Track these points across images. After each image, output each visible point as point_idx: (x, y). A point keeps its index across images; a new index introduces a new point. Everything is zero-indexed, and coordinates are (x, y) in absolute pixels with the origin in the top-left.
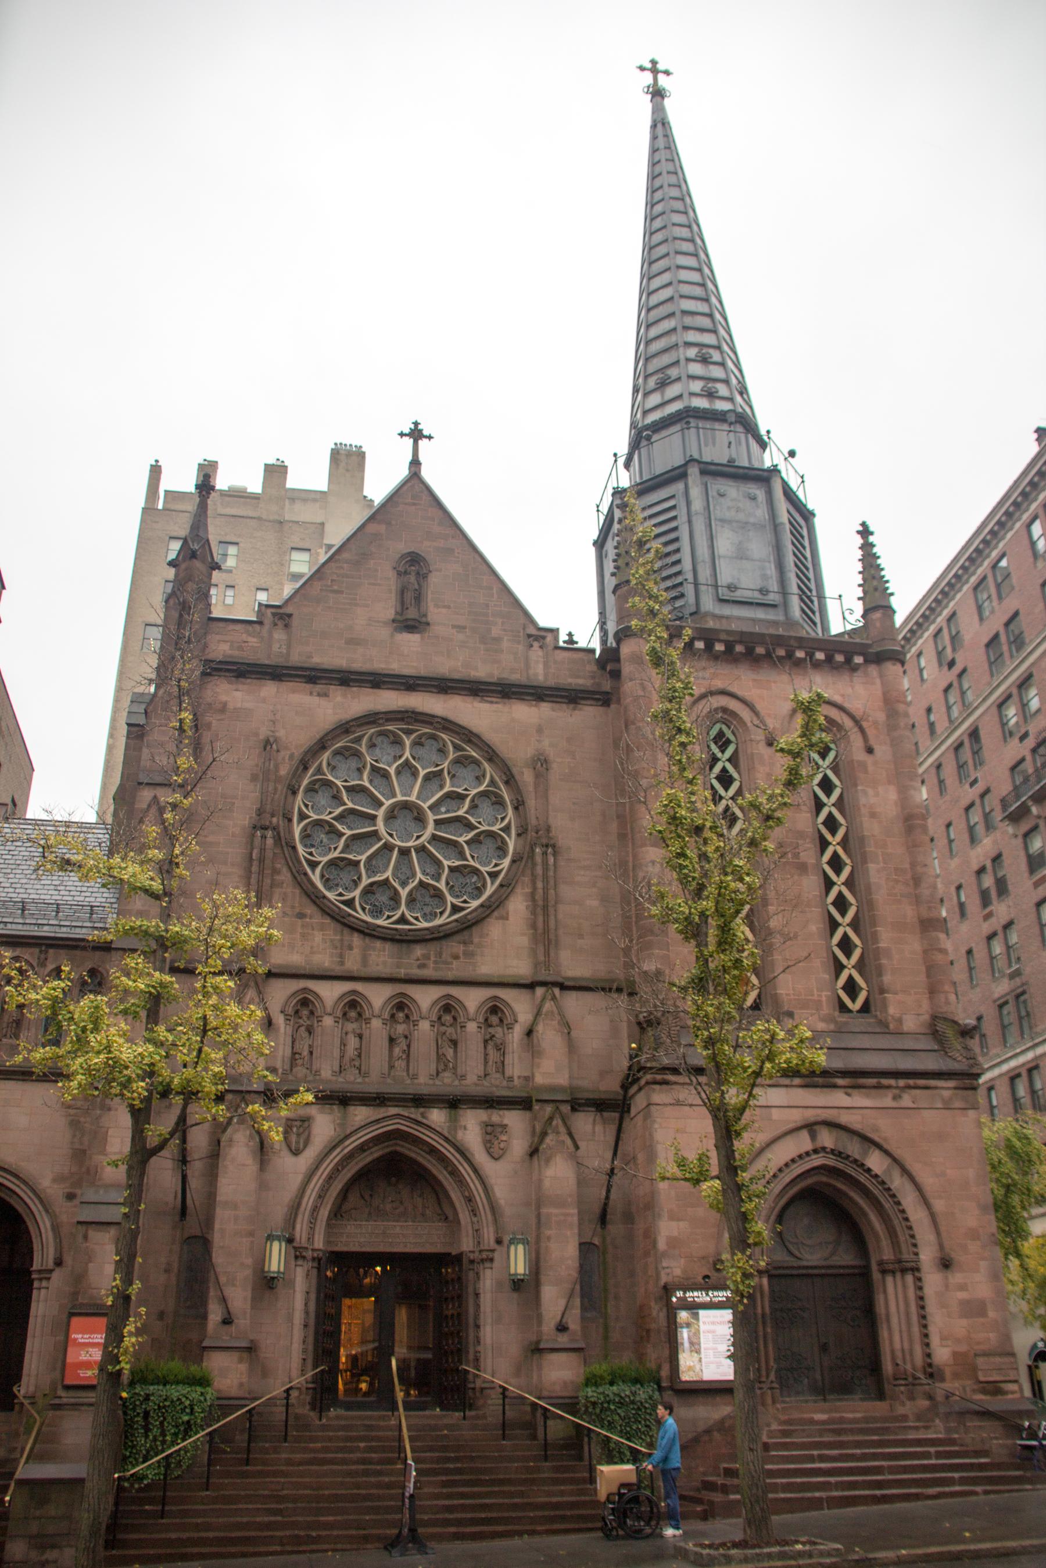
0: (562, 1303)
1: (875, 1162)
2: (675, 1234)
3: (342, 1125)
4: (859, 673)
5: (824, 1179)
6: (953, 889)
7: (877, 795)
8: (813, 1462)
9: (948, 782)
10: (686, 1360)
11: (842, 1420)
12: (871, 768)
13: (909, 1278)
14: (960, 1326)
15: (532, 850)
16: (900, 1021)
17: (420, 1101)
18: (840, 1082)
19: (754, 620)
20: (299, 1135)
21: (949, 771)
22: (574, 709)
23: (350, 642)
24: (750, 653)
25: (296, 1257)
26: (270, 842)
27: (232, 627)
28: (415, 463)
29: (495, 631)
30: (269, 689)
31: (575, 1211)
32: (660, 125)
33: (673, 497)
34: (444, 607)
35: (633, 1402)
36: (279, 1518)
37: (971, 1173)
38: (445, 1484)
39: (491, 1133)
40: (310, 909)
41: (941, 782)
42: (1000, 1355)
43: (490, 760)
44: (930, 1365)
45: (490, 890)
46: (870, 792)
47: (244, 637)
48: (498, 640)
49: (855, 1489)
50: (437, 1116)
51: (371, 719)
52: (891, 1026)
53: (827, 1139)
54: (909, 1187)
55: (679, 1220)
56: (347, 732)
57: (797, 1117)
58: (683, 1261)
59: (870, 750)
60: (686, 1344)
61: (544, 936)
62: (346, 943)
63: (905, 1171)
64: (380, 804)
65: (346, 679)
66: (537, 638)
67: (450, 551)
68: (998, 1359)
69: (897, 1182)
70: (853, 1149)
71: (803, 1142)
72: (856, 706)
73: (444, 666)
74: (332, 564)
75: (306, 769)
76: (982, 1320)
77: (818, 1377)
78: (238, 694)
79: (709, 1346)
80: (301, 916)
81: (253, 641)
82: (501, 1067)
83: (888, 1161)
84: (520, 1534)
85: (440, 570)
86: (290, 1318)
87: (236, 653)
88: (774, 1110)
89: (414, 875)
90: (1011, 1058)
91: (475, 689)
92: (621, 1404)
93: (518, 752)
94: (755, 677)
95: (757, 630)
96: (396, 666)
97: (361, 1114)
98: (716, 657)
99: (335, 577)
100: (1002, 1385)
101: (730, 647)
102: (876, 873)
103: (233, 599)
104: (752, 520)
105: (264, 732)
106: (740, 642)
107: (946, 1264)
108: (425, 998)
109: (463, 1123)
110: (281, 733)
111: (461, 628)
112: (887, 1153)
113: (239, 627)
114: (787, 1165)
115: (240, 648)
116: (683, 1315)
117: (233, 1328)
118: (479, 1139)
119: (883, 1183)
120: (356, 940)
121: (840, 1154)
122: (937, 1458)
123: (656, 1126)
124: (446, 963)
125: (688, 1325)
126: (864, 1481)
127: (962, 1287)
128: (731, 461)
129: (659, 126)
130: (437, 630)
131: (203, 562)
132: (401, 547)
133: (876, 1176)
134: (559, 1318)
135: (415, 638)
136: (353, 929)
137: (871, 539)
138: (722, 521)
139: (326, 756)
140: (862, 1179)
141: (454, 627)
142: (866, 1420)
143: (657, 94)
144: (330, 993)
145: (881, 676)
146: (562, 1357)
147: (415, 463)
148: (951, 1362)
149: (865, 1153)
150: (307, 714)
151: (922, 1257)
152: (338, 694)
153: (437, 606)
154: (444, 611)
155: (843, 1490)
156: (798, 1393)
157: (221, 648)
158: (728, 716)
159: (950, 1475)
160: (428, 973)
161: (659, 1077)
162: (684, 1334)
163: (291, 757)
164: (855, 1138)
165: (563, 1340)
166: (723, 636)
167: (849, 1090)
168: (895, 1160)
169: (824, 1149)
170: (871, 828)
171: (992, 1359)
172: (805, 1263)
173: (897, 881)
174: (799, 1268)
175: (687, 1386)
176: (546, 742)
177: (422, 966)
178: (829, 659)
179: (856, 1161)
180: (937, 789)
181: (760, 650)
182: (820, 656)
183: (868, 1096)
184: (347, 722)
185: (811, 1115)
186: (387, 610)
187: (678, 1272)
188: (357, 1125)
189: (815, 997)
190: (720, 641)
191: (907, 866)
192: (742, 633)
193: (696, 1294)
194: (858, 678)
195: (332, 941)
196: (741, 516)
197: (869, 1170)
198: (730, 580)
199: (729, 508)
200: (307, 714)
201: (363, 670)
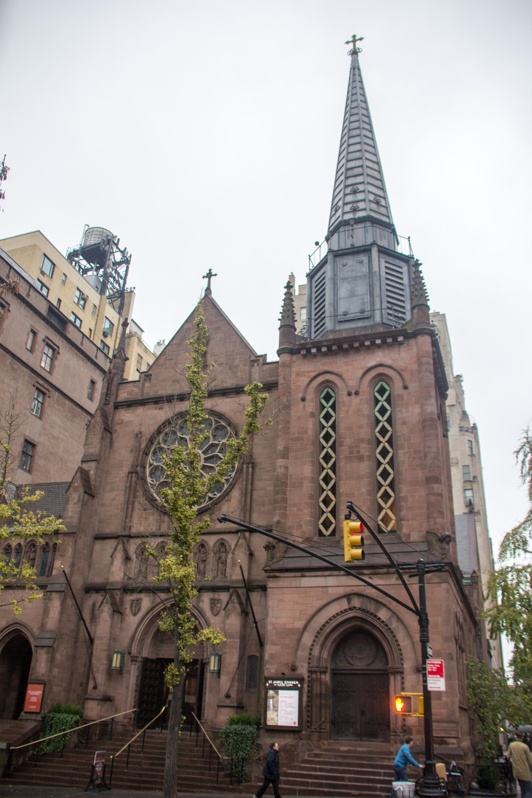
0: (229, 684)
2: (274, 652)
3: (153, 602)
4: (404, 345)
5: (359, 623)
7: (408, 411)
8: (316, 771)
10: (270, 714)
11: (355, 752)
12: (405, 397)
13: (399, 677)
15: (242, 466)
16: (409, 536)
18: (366, 572)
19: (354, 329)
20: (136, 607)
24: (340, 348)
25: (132, 661)
26: (134, 478)
28: (208, 290)
29: (236, 362)
30: (140, 410)
31: (238, 640)
32: (355, 69)
35: (242, 734)
36: (77, 772)
38: (152, 764)
39: (214, 602)
42: (447, 722)
43: (229, 425)
44: (404, 725)
45: (226, 486)
46: (404, 410)
49: (322, 787)
53: (356, 602)
54: (401, 627)
55: (276, 645)
57: (341, 591)
58: (276, 665)
59: (406, 388)
60: (271, 707)
61: (247, 506)
65: (169, 399)
66: (255, 361)
68: (445, 725)
69: (394, 625)
70: (371, 607)
71: (344, 604)
72: (400, 364)
74: (169, 347)
75: (152, 443)
77: (358, 728)
78: (128, 415)
79: (285, 708)
81: (136, 390)
82: (224, 573)
83: (389, 614)
84: (155, 789)
85: (214, 339)
86: (128, 687)
87: (129, 396)
88: (329, 589)
92: (236, 734)
94: (345, 360)
95: (357, 333)
98: (325, 354)
100: (446, 739)
101: (329, 348)
102: (402, 456)
104: (359, 274)
105: (137, 430)
106: (334, 344)
109: (202, 599)
110: (143, 429)
112: (389, 609)
114: (334, 617)
115: (131, 394)
116: (271, 692)
117: (97, 691)
118: (209, 607)
119: (387, 625)
121: (364, 610)
122: (384, 776)
123: (269, 598)
125: (273, 697)
126: (326, 783)
128: (353, 245)
129: (356, 70)
131: (120, 359)
133: (383, 622)
134: (227, 691)
138: (343, 279)
139: (161, 437)
140: (375, 623)
142: (369, 752)
143: (355, 53)
145: (417, 344)
147: (208, 290)
148: (417, 724)
149: (377, 610)
150: (152, 417)
151: (405, 666)
155: (314, 787)
156: (347, 736)
157: (123, 395)
158: (327, 383)
159: (375, 785)
161: (272, 574)
162: (271, 702)
163: (146, 439)
164: (373, 601)
165: (228, 702)
166: (325, 343)
167: (371, 576)
168: (394, 613)
169: (355, 608)
170: (401, 430)
171: (441, 724)
172: (356, 668)
173: (414, 458)
174: (351, 670)
175: (269, 728)
178: (384, 342)
179: (372, 614)
181: (345, 346)
182: (378, 342)
183: (381, 578)
185: (348, 590)
187: (273, 671)
190: (324, 346)
191: (422, 449)
192: (334, 339)
193: (278, 682)
194: (403, 349)
196: (354, 274)
197: (379, 619)
198: (344, 310)
200: (152, 417)
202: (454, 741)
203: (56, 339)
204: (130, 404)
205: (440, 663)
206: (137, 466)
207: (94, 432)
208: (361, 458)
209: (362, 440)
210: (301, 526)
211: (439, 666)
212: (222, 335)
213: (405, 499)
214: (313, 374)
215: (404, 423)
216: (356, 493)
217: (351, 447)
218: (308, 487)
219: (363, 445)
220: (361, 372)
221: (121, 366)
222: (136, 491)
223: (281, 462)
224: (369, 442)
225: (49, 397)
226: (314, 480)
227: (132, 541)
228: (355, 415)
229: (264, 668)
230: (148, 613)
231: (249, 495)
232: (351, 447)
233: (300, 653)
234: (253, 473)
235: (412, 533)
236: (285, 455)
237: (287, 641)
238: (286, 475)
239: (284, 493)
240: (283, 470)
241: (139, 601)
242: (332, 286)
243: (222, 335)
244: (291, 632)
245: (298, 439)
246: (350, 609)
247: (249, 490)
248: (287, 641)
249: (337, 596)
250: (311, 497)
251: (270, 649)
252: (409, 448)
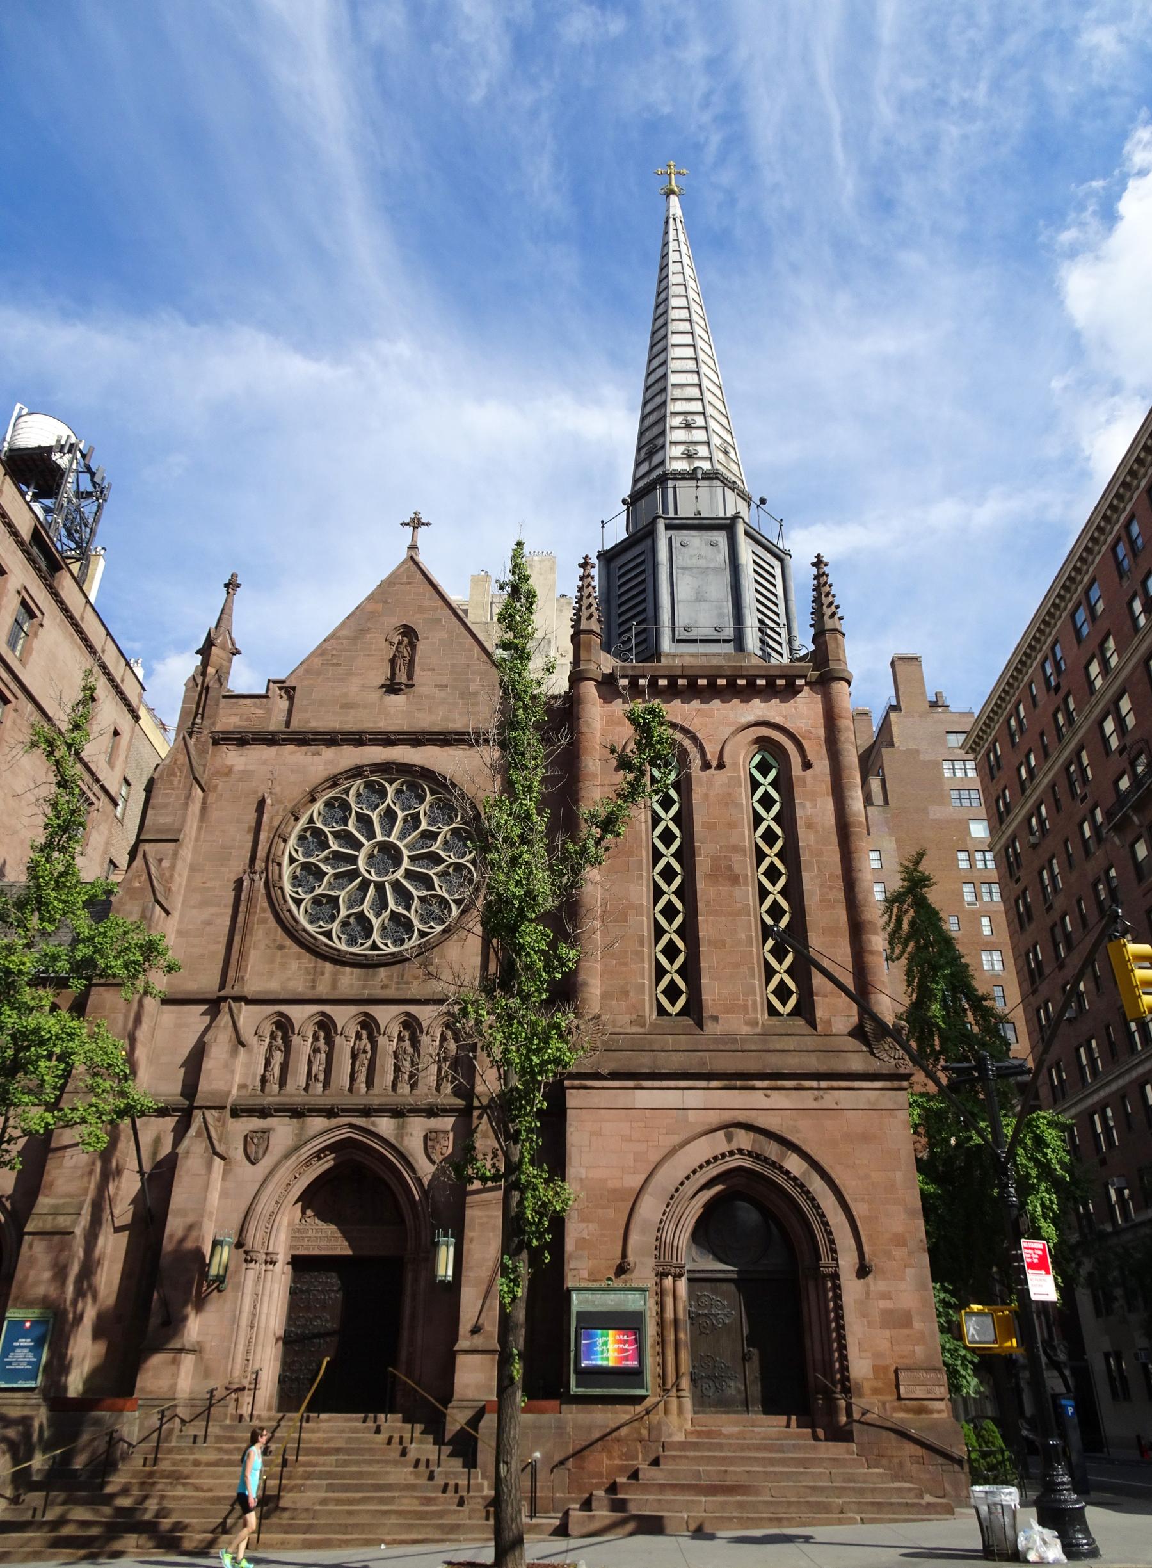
1: (794, 1164)
3: (299, 1135)
6: (1074, 902)
7: (815, 807)
9: (1063, 801)
14: (882, 1339)
16: (829, 1023)
17: (367, 1112)
18: (758, 1084)
21: (1062, 790)
23: (346, 706)
27: (242, 701)
28: (413, 547)
33: (643, 552)
34: (429, 670)
37: (899, 1176)
40: (289, 942)
41: (1057, 801)
46: (808, 804)
47: (253, 710)
48: (475, 694)
50: (385, 1126)
51: (356, 772)
52: (819, 1028)
56: (335, 785)
57: (715, 1118)
62: (318, 970)
69: (817, 1185)
70: (772, 1150)
71: (718, 1143)
73: (425, 721)
76: (906, 1331)
81: (260, 712)
85: (427, 638)
87: (245, 724)
89: (362, 903)
90: (1138, 1064)
91: (445, 739)
96: (383, 725)
97: (318, 1123)
99: (334, 652)
103: (244, 678)
104: (712, 565)
108: (385, 1015)
109: (409, 1130)
111: (442, 687)
113: (248, 701)
120: (328, 966)
124: (407, 983)
127: (886, 1296)
132: (397, 621)
133: (795, 1179)
135: (400, 699)
136: (325, 958)
137: (826, 569)
138: (684, 568)
141: (436, 686)
144: (299, 1014)
146: (477, 1358)
147: (413, 547)
149: (783, 1156)
152: (328, 753)
154: (429, 673)
157: (228, 719)
160: (390, 993)
167: (769, 1092)
169: (740, 1151)
173: (831, 888)
177: (384, 987)
179: (774, 1164)
180: (1054, 808)
184: (335, 776)
185: (728, 1116)
186: (381, 675)
188: (312, 1133)
189: (741, 1002)
195: (306, 968)
196: (703, 563)
197: (787, 1173)
199: (691, 557)
201: (354, 730)
203: (41, 596)
204: (241, 739)
205: (1041, 1246)
207: (171, 782)
210: (627, 994)
211: (1040, 1253)
212: (444, 635)
215: (810, 826)
216: (728, 940)
217: (715, 859)
221: (225, 663)
225: (16, 710)
229: (566, 1268)
230: (287, 1156)
232: (715, 859)
235: (833, 1019)
237: (611, 1213)
243: (444, 635)
244: (616, 1194)
248: (611, 1213)
249: (707, 1127)
251: (574, 1232)
252: (819, 869)
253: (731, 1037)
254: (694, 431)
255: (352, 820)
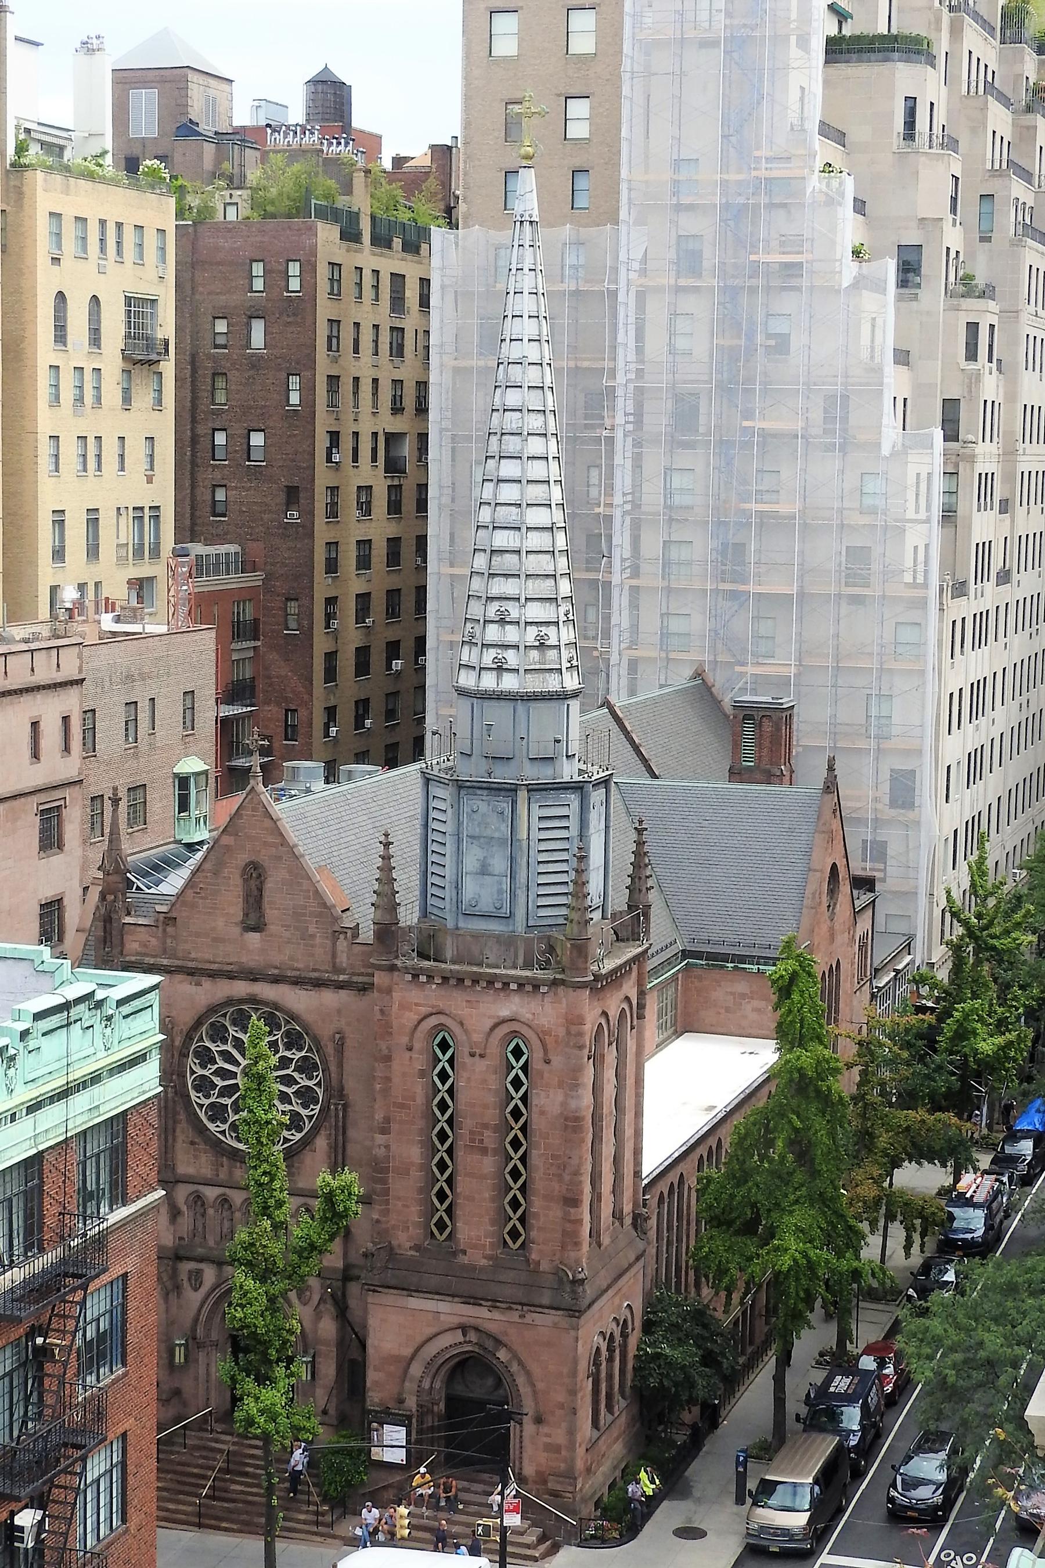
7: (548, 1097)
12: (546, 1075)
14: (543, 1457)
16: (538, 1263)
22: (364, 995)
23: (215, 940)
29: (312, 930)
46: (543, 1094)
51: (230, 1002)
57: (456, 1320)
59: (548, 1062)
63: (521, 1363)
64: (238, 1064)
67: (280, 858)
69: (515, 1368)
70: (489, 1344)
76: (556, 1455)
80: (192, 1143)
86: (196, 1379)
93: (325, 1031)
102: (536, 1158)
107: (539, 1420)
115: (145, 946)
130: (272, 928)
141: (282, 926)
144: (211, 1193)
149: (497, 1350)
152: (207, 983)
153: (271, 908)
170: (538, 1123)
173: (552, 1165)
176: (343, 1023)
183: (503, 1313)
185: (464, 1320)
186: (236, 910)
202: (570, 1495)
206: (172, 1074)
208: (484, 1151)
209: (485, 1126)
213: (536, 1215)
214: (424, 1010)
218: (416, 1176)
219: (487, 1133)
220: (489, 1023)
222: (175, 1113)
223: (380, 1139)
224: (496, 1129)
226: (426, 1167)
227: (181, 1186)
228: (478, 1086)
231: (340, 1151)
233: (407, 1384)
234: (344, 1117)
236: (385, 1131)
238: (387, 1158)
239: (384, 1181)
240: (383, 1149)
241: (199, 1273)
242: (454, 849)
244: (396, 1359)
245: (402, 1106)
246: (465, 1342)
247: (340, 1145)
250: (421, 1191)
253: (473, 1268)
254: (508, 627)
255: (217, 1080)
